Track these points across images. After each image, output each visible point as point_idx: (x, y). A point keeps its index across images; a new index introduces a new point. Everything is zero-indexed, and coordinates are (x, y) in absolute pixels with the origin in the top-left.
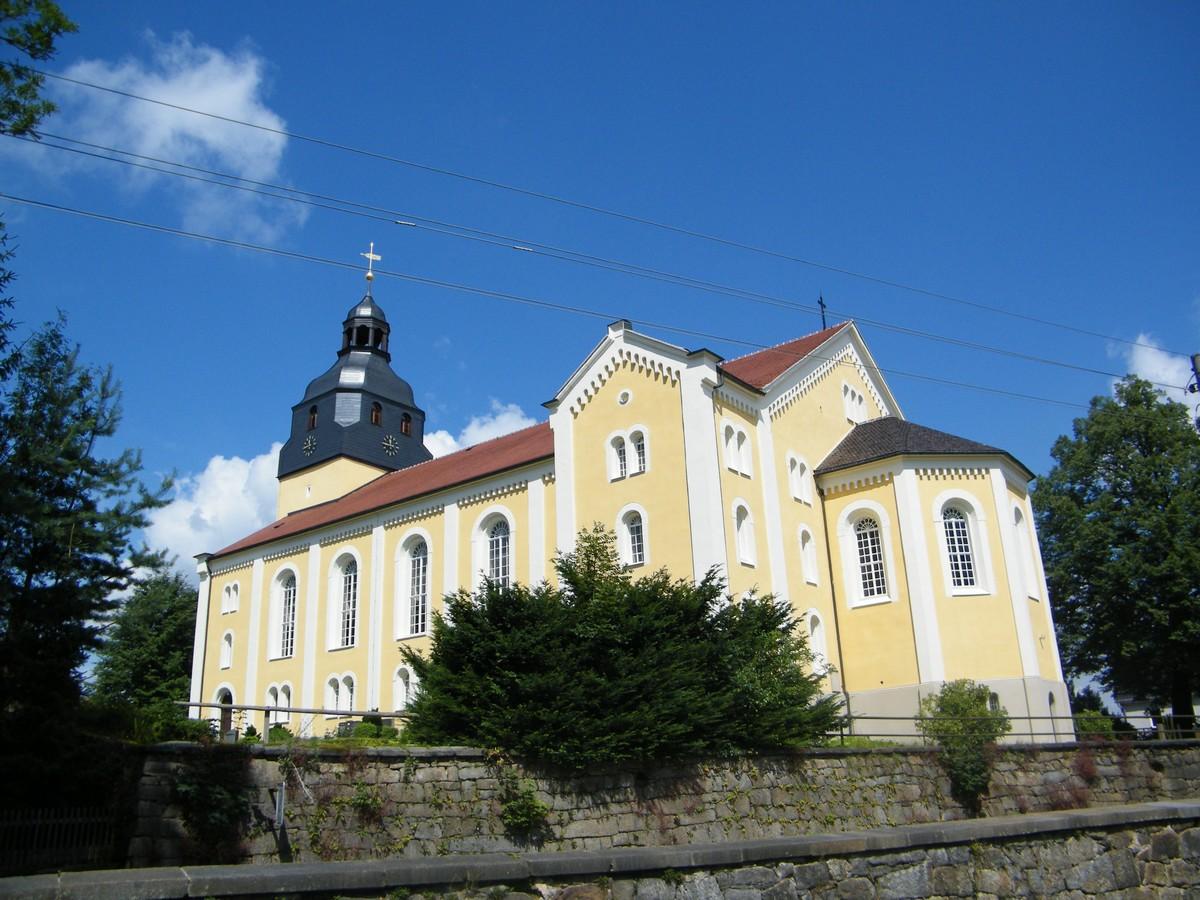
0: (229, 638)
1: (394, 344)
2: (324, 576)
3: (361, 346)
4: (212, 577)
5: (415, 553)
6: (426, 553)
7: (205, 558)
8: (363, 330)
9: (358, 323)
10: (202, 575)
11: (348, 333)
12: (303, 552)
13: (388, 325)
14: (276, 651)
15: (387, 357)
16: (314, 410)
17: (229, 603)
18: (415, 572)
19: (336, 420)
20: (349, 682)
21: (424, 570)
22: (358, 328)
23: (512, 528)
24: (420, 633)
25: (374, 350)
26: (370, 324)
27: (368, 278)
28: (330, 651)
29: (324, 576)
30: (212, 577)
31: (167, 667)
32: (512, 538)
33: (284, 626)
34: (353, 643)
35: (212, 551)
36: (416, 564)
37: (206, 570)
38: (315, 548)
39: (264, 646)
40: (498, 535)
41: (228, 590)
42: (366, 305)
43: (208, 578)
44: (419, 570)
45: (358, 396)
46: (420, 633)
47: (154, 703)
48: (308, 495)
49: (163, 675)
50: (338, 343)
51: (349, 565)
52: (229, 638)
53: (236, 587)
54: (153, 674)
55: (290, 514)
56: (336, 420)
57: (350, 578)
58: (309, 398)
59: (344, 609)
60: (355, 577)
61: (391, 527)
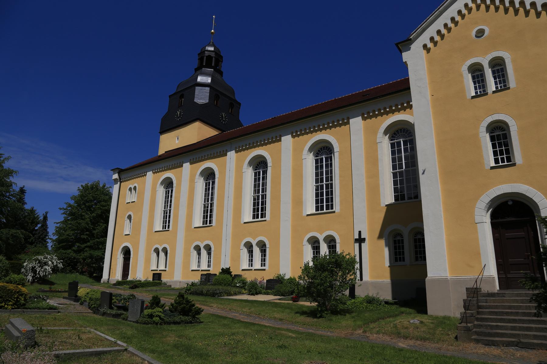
0: (130, 217)
1: (224, 67)
2: (192, 181)
3: (209, 66)
4: (121, 182)
5: (207, 178)
6: (172, 187)
7: (118, 171)
8: (209, 58)
9: (207, 53)
10: (116, 181)
11: (201, 59)
12: (143, 176)
13: (222, 57)
14: (158, 226)
15: (221, 73)
16: (182, 96)
17: (131, 197)
18: (207, 190)
19: (195, 101)
20: (208, 248)
21: (213, 188)
22: (207, 56)
23: (270, 164)
24: (260, 219)
25: (215, 68)
26: (213, 55)
27: (212, 33)
28: (195, 228)
29: (192, 181)
30: (121, 182)
31: (95, 232)
32: (217, 180)
33: (164, 211)
34: (168, 228)
35: (123, 168)
36: (207, 185)
37: (118, 178)
38: (150, 174)
39: (298, 202)
40: (210, 180)
41: (130, 189)
42: (211, 46)
43: (119, 183)
44: (168, 196)
45: (208, 89)
46: (260, 219)
47: (86, 251)
48: (177, 142)
49: (92, 236)
50: (196, 64)
51: (168, 184)
52: (130, 217)
53: (135, 188)
54: (87, 235)
55: (166, 152)
56: (195, 101)
57: (169, 191)
58: (180, 90)
59: (165, 208)
60: (172, 191)
61: (156, 173)
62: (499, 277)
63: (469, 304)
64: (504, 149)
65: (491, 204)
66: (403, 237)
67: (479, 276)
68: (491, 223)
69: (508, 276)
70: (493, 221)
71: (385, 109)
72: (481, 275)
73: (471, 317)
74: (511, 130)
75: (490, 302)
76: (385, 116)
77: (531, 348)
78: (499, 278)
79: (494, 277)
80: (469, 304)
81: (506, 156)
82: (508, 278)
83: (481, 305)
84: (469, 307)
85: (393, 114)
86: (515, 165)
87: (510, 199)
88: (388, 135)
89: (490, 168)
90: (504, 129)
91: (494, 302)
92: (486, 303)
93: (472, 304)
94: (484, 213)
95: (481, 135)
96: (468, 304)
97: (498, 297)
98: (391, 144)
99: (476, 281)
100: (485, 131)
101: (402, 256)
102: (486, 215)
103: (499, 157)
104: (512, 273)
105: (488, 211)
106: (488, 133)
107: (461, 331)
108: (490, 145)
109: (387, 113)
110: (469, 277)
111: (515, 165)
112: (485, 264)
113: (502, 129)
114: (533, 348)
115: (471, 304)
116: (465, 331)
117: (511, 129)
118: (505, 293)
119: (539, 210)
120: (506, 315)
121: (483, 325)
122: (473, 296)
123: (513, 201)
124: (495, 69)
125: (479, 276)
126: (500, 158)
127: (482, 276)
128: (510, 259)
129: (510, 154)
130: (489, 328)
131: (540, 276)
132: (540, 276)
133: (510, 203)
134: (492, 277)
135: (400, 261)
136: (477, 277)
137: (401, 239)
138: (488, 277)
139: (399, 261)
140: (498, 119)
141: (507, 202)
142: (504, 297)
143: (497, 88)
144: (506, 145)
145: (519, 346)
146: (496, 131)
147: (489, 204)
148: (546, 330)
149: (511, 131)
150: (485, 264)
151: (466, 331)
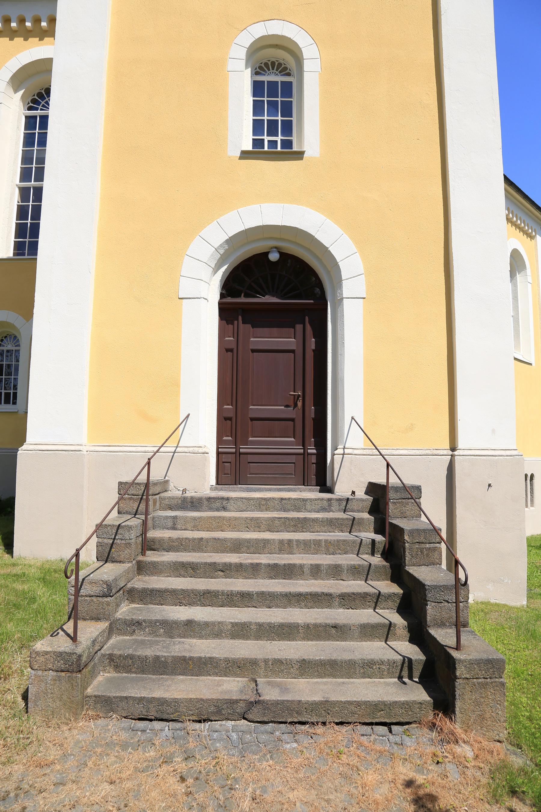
62: (220, 450)
63: (114, 539)
64: (281, 120)
65: (226, 251)
66: (19, 345)
67: (162, 446)
68: (220, 304)
69: (241, 450)
70: (224, 300)
71: (22, 21)
72: (172, 443)
73: (105, 596)
74: (306, 68)
75: (184, 527)
76: (19, 40)
77: (289, 720)
78: (218, 454)
79: (207, 451)
80: (114, 539)
81: (281, 140)
82: (240, 454)
83: (153, 540)
84: (113, 550)
85: (41, 39)
86: (302, 159)
87: (276, 248)
88: (24, 90)
89: (238, 154)
90: (288, 71)
91: (196, 528)
92: (174, 528)
93: (123, 542)
94: (205, 272)
95: (231, 65)
96: (111, 541)
97: (211, 509)
98: (26, 117)
99: (149, 463)
100: (244, 57)
101: (12, 391)
102: (210, 280)
103: (266, 138)
104: (253, 443)
105: (216, 270)
106: (249, 69)
107: (46, 673)
108: (249, 100)
109: (27, 34)
110: (140, 449)
111: (302, 159)
112: (189, 415)
113: (284, 70)
114: (296, 720)
115: (119, 541)
116: (62, 671)
117: (307, 66)
118: (228, 499)
119: (340, 280)
120: (221, 573)
121: (144, 621)
122: (136, 508)
123: (282, 254)
124: (265, 78)
125: (162, 446)
126: (269, 141)
127: (177, 447)
128: (254, 405)
129: (292, 136)
130: (162, 630)
131: (315, 451)
132: (315, 451)
133: (274, 257)
134: (201, 450)
135: (7, 402)
136: (173, 449)
137: (14, 348)
138: (191, 449)
139: (5, 403)
140: (279, 33)
141: (266, 254)
142: (224, 509)
143: (258, 143)
144: (287, 110)
145: (250, 716)
146: (268, 72)
147: (222, 251)
148: (333, 631)
149: (305, 70)
150: (189, 415)
151: (63, 674)
